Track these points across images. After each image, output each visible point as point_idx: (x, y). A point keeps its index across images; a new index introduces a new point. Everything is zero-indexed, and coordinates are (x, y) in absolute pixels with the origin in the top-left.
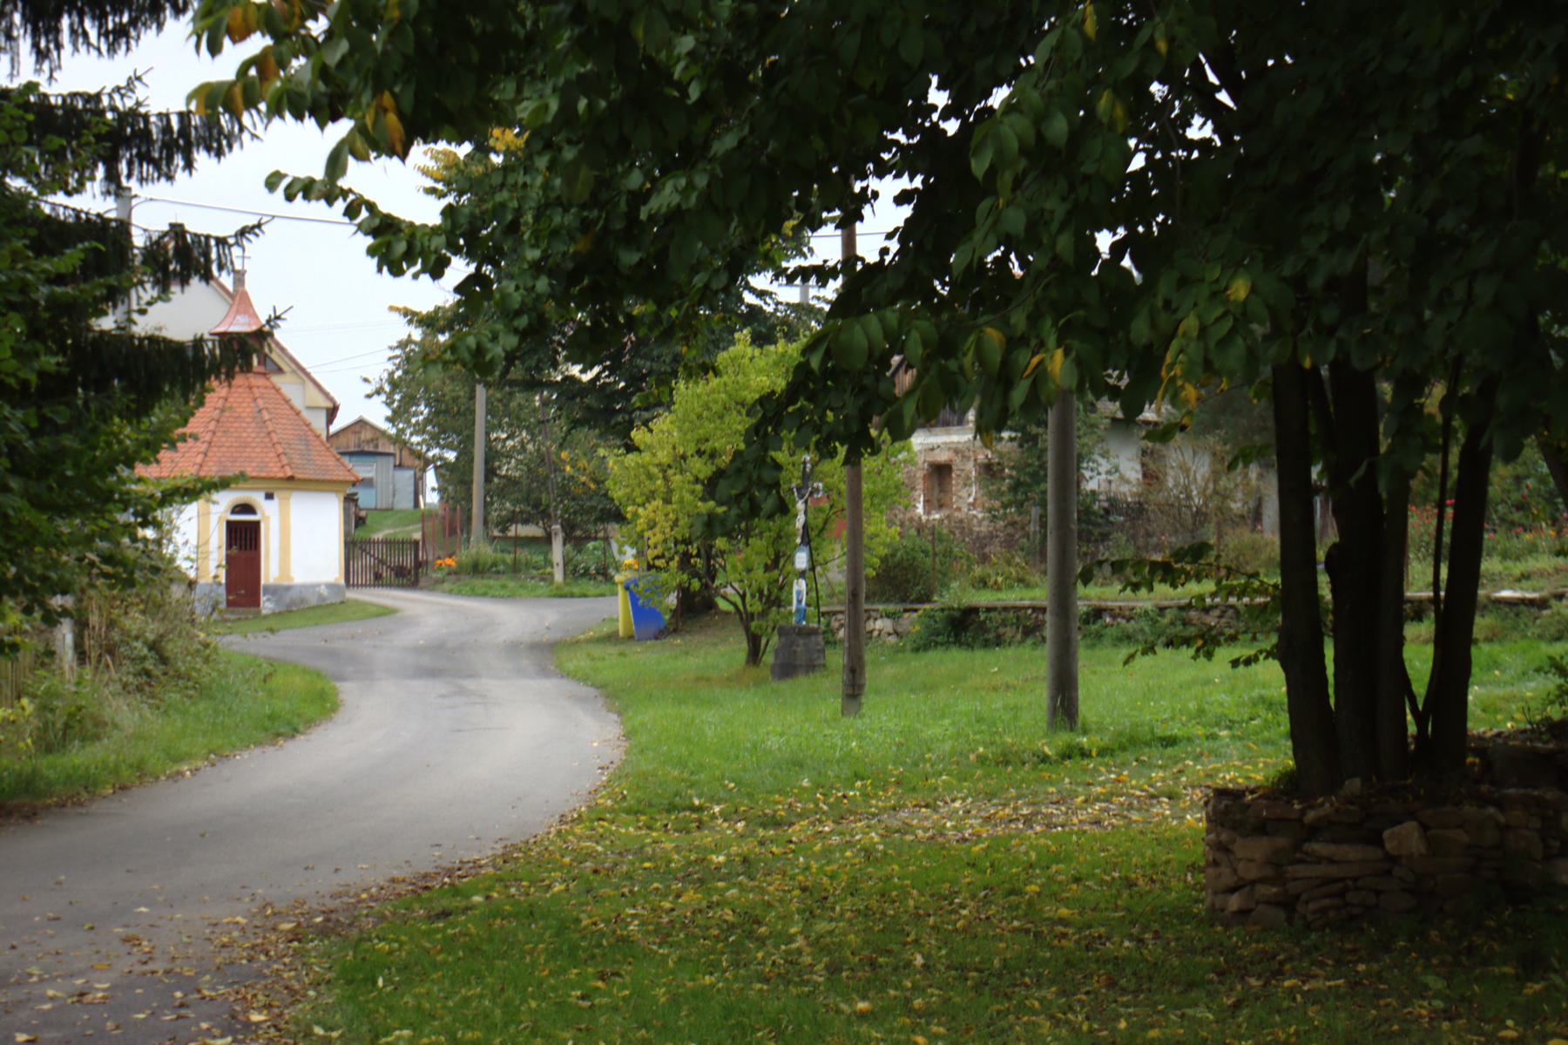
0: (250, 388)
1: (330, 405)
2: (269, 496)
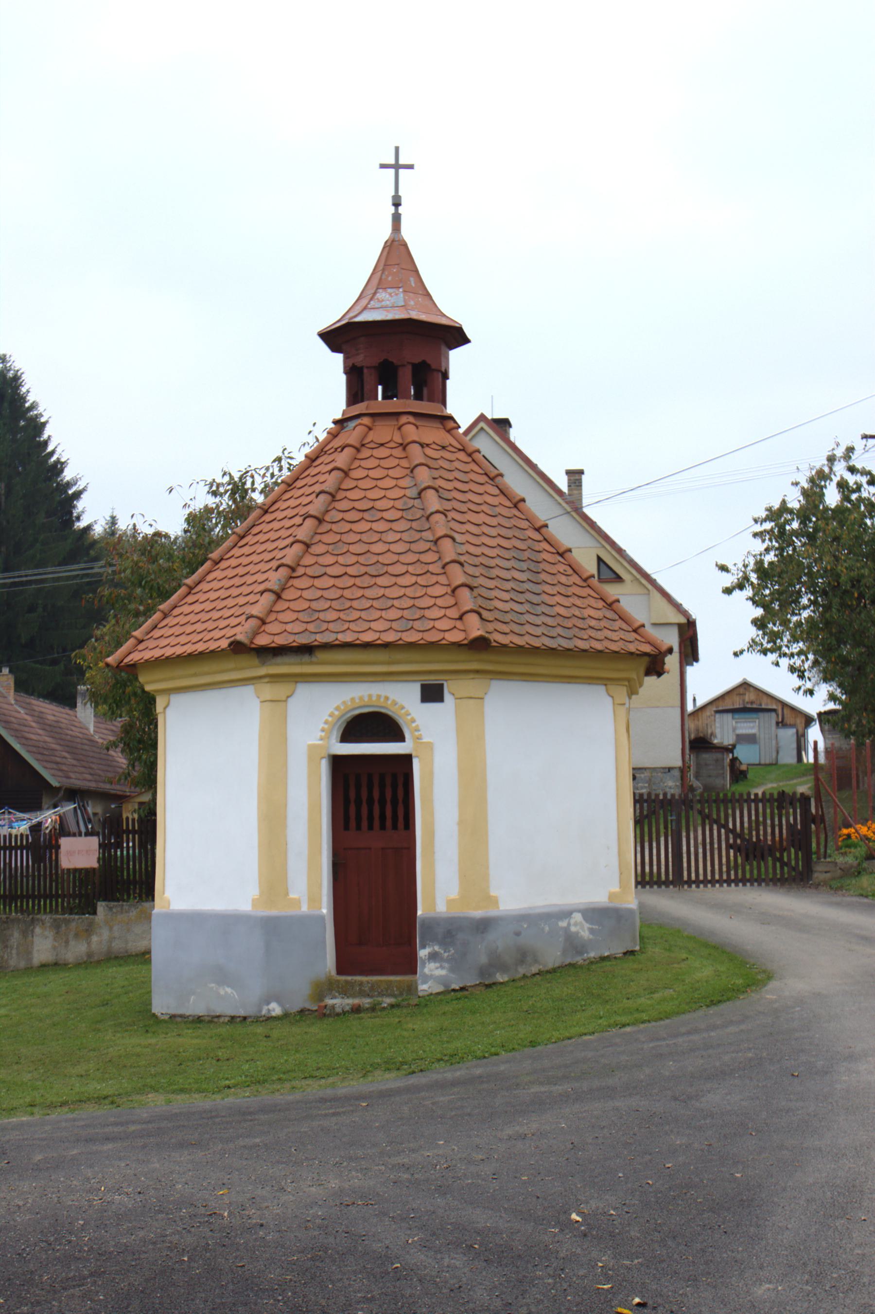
0: (404, 446)
1: (683, 620)
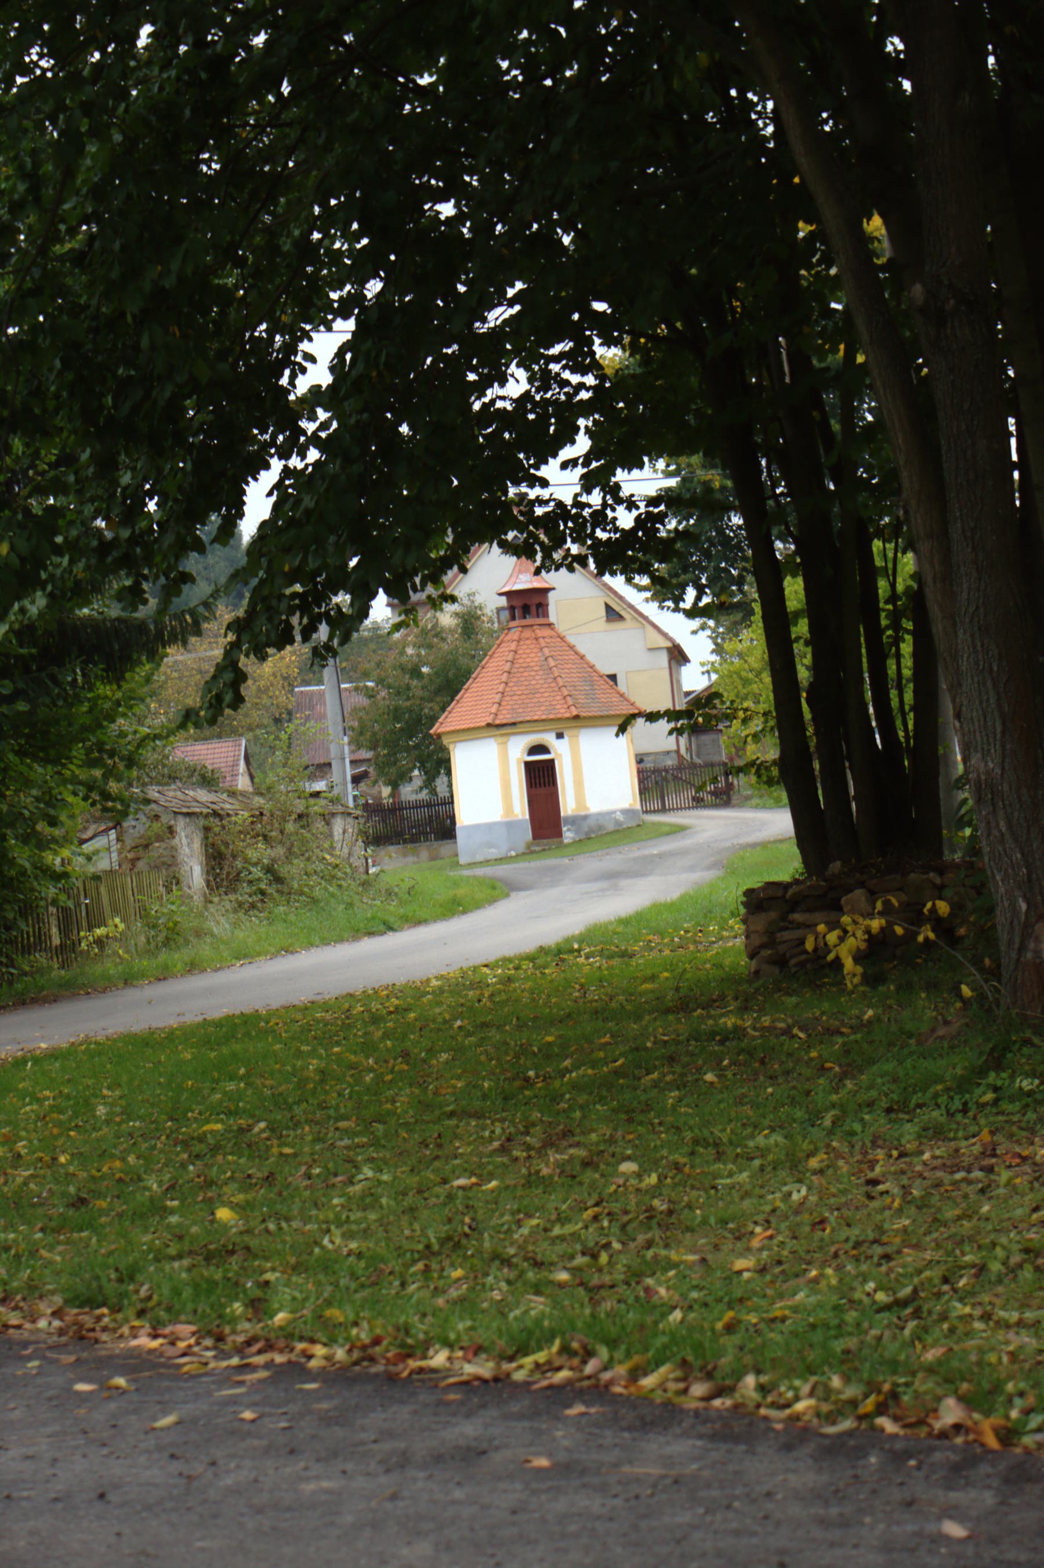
0: (537, 639)
2: (560, 736)
